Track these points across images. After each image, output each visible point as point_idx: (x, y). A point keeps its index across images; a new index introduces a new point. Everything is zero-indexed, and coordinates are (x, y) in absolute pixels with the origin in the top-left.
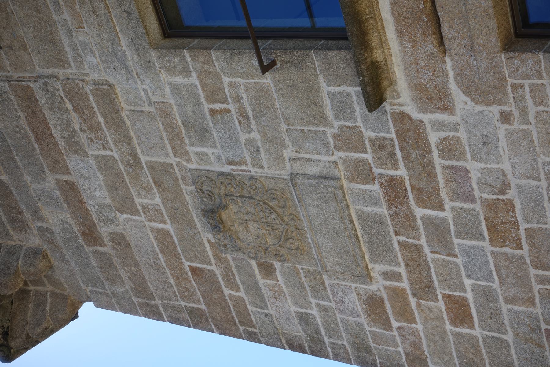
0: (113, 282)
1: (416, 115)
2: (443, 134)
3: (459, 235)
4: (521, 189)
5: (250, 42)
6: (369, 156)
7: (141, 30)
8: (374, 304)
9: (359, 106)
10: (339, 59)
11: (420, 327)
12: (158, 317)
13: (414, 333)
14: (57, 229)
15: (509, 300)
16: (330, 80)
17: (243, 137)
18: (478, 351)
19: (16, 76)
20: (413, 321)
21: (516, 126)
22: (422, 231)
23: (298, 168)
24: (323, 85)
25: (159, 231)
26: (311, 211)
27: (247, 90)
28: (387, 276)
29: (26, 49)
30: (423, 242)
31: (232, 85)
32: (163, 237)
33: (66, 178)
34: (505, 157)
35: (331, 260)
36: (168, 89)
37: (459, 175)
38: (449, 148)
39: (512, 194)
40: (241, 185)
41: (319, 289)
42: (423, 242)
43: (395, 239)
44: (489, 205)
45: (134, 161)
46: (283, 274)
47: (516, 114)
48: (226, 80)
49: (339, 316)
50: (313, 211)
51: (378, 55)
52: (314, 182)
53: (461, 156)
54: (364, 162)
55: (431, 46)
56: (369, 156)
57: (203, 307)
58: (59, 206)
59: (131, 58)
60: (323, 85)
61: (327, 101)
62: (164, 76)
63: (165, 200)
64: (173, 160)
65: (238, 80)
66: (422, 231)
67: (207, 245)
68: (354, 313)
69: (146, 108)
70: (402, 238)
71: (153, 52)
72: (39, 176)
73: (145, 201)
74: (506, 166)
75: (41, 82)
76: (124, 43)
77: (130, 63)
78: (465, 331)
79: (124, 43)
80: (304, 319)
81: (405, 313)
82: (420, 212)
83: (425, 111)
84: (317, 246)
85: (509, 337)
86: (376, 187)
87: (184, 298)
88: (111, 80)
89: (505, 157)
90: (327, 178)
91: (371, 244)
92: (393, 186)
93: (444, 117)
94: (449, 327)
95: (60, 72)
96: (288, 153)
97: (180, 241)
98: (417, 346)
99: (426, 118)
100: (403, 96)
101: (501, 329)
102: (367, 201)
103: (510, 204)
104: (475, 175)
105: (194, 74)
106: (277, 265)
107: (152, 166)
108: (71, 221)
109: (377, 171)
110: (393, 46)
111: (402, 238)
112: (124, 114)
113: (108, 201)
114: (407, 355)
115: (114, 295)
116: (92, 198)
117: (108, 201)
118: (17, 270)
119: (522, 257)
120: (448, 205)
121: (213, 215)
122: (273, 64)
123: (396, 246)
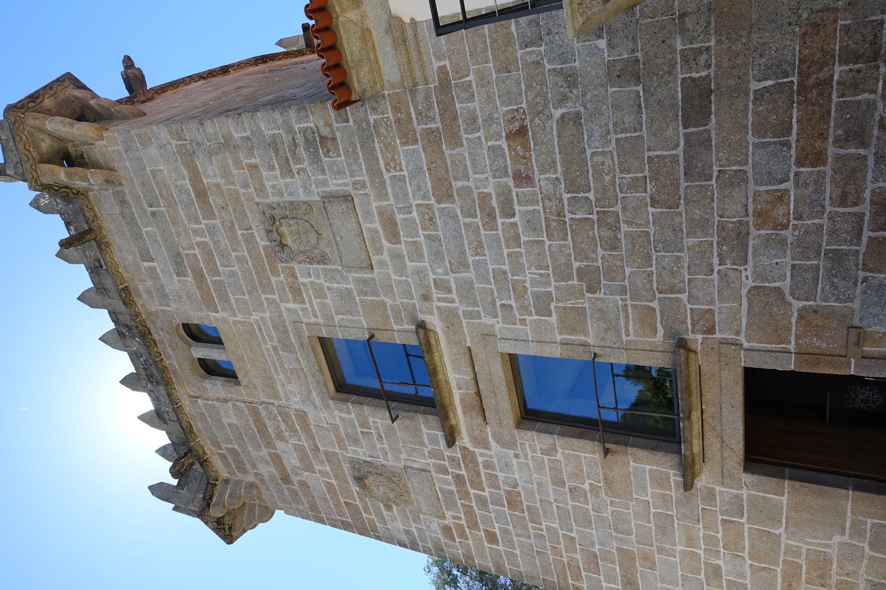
0: (298, 503)
1: (471, 449)
2: (485, 459)
3: (492, 504)
4: (524, 488)
5: (384, 401)
6: (447, 463)
7: (325, 390)
8: (446, 530)
9: (442, 442)
10: (433, 420)
11: (471, 542)
12: (324, 523)
13: (468, 545)
14: (266, 475)
15: (517, 535)
16: (428, 429)
17: (379, 446)
18: (501, 557)
19: (248, 400)
20: (468, 539)
21: (522, 460)
22: (473, 499)
23: (408, 464)
24: (423, 429)
25: (328, 482)
26: (414, 484)
27: (382, 425)
28: (454, 517)
29: (256, 388)
30: (474, 504)
31: (373, 422)
32: (330, 486)
33: (274, 451)
34: (516, 473)
35: (424, 508)
36: (338, 419)
37: (493, 479)
38: (487, 465)
39: (519, 489)
40: (376, 468)
41: (416, 519)
42: (474, 504)
43: (459, 502)
44: (508, 493)
45: (316, 449)
46: (397, 510)
47: (522, 455)
48: (371, 419)
49: (427, 533)
50: (416, 485)
51: (453, 422)
52: (417, 472)
53: (494, 469)
54: (444, 466)
55: (480, 420)
56: (447, 463)
57: (350, 520)
58: (269, 464)
59: (318, 402)
60: (423, 429)
61: (425, 436)
62: (336, 412)
63: (332, 469)
64: (338, 451)
65: (378, 420)
66: (473, 499)
67: (355, 493)
68: (435, 532)
69: (325, 425)
70: (463, 502)
71: (330, 401)
72: (258, 448)
73: (320, 468)
74: (517, 477)
75: (264, 406)
76: (314, 394)
77: (317, 404)
78: (494, 547)
79: (314, 394)
80: (408, 532)
81: (463, 535)
82: (472, 491)
83: (477, 448)
84: (417, 501)
85: (518, 552)
86: (450, 477)
87: (339, 515)
88: (305, 410)
89: (516, 473)
90: (424, 470)
91: (446, 503)
92: (459, 479)
93: (486, 452)
94: (486, 544)
95: (276, 402)
96: (403, 456)
97: (339, 489)
98: (469, 551)
99: (477, 451)
100: (465, 439)
101: (513, 547)
102: (445, 483)
103: (519, 494)
104: (501, 479)
105: (282, 275)
106: (394, 506)
107: (326, 453)
108: (274, 471)
109: (450, 470)
110: (461, 418)
111: (463, 502)
112: (312, 427)
113: (298, 465)
114: (464, 555)
115: (297, 509)
116: (290, 462)
117: (298, 465)
118: (240, 495)
119: (524, 517)
120: (487, 490)
121: (360, 480)
122: (397, 417)
123: (460, 505)
